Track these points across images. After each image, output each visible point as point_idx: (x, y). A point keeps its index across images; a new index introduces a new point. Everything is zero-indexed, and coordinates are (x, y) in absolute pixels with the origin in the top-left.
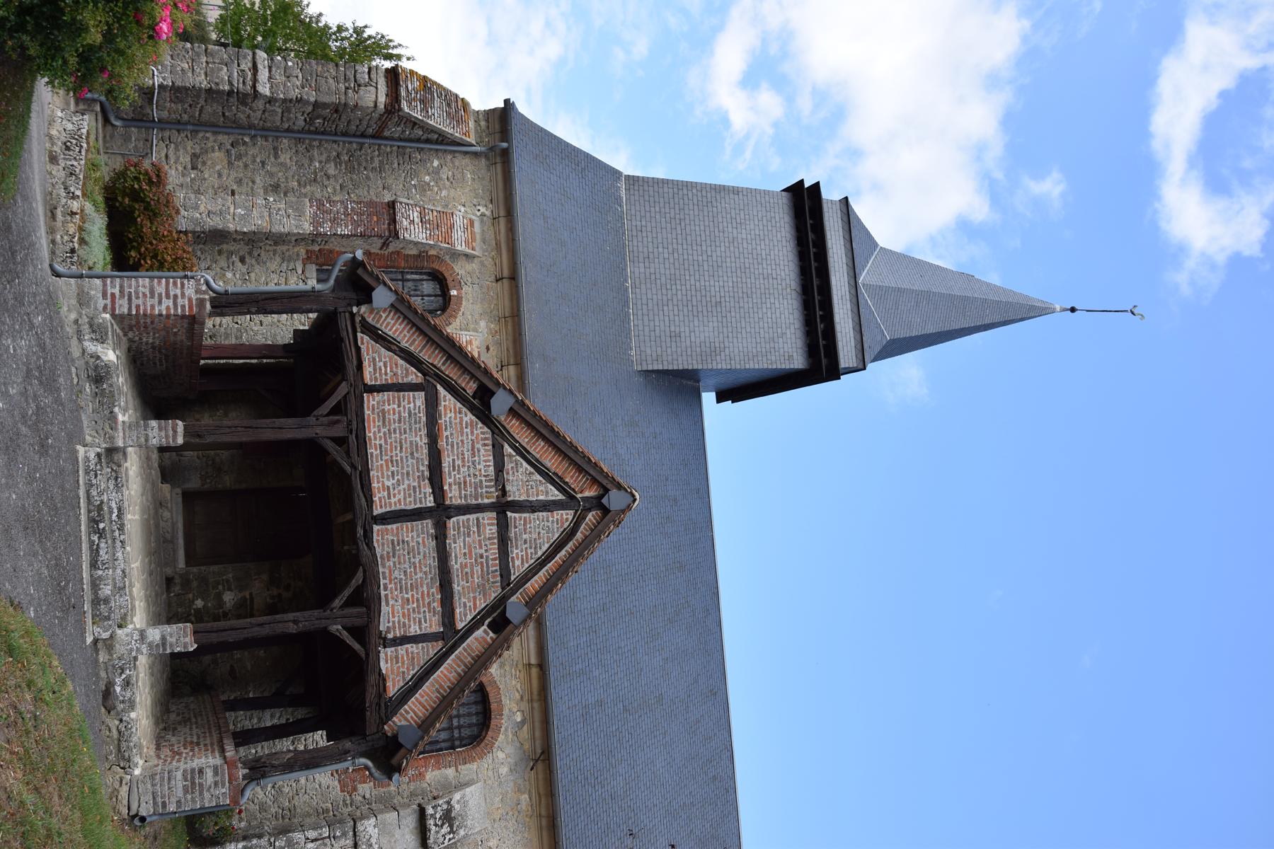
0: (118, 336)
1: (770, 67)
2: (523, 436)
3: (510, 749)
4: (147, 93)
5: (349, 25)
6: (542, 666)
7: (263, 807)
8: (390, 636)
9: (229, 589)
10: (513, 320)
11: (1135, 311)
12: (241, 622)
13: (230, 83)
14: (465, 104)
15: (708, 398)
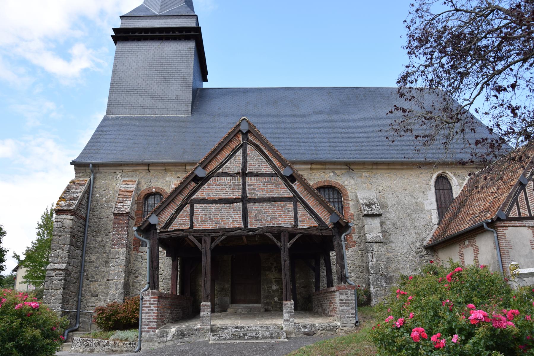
0: (165, 327)
1: (62, 49)
2: (215, 164)
3: (344, 179)
4: (64, 313)
5: (37, 230)
6: (312, 163)
7: (358, 278)
8: (294, 223)
9: (271, 287)
10: (166, 166)
12: (284, 282)
13: (61, 280)
14: (72, 182)
15: (205, 85)
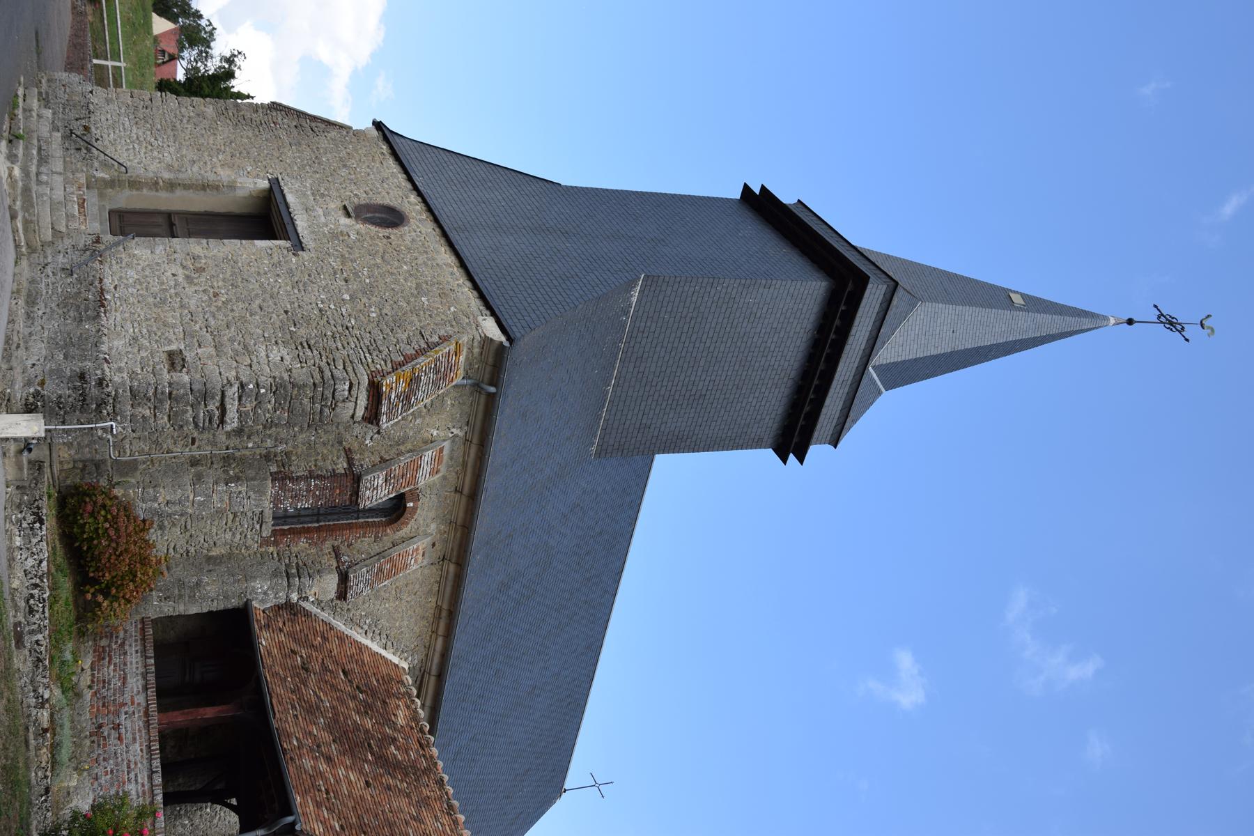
11: (1206, 323)
